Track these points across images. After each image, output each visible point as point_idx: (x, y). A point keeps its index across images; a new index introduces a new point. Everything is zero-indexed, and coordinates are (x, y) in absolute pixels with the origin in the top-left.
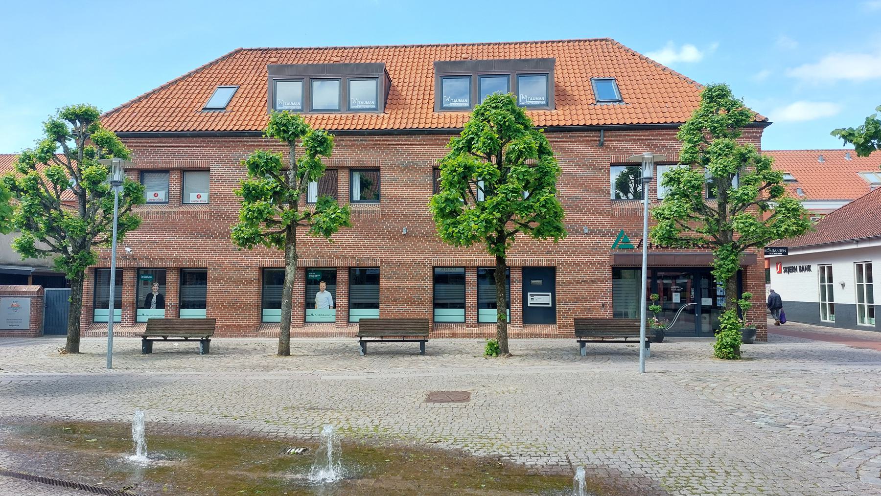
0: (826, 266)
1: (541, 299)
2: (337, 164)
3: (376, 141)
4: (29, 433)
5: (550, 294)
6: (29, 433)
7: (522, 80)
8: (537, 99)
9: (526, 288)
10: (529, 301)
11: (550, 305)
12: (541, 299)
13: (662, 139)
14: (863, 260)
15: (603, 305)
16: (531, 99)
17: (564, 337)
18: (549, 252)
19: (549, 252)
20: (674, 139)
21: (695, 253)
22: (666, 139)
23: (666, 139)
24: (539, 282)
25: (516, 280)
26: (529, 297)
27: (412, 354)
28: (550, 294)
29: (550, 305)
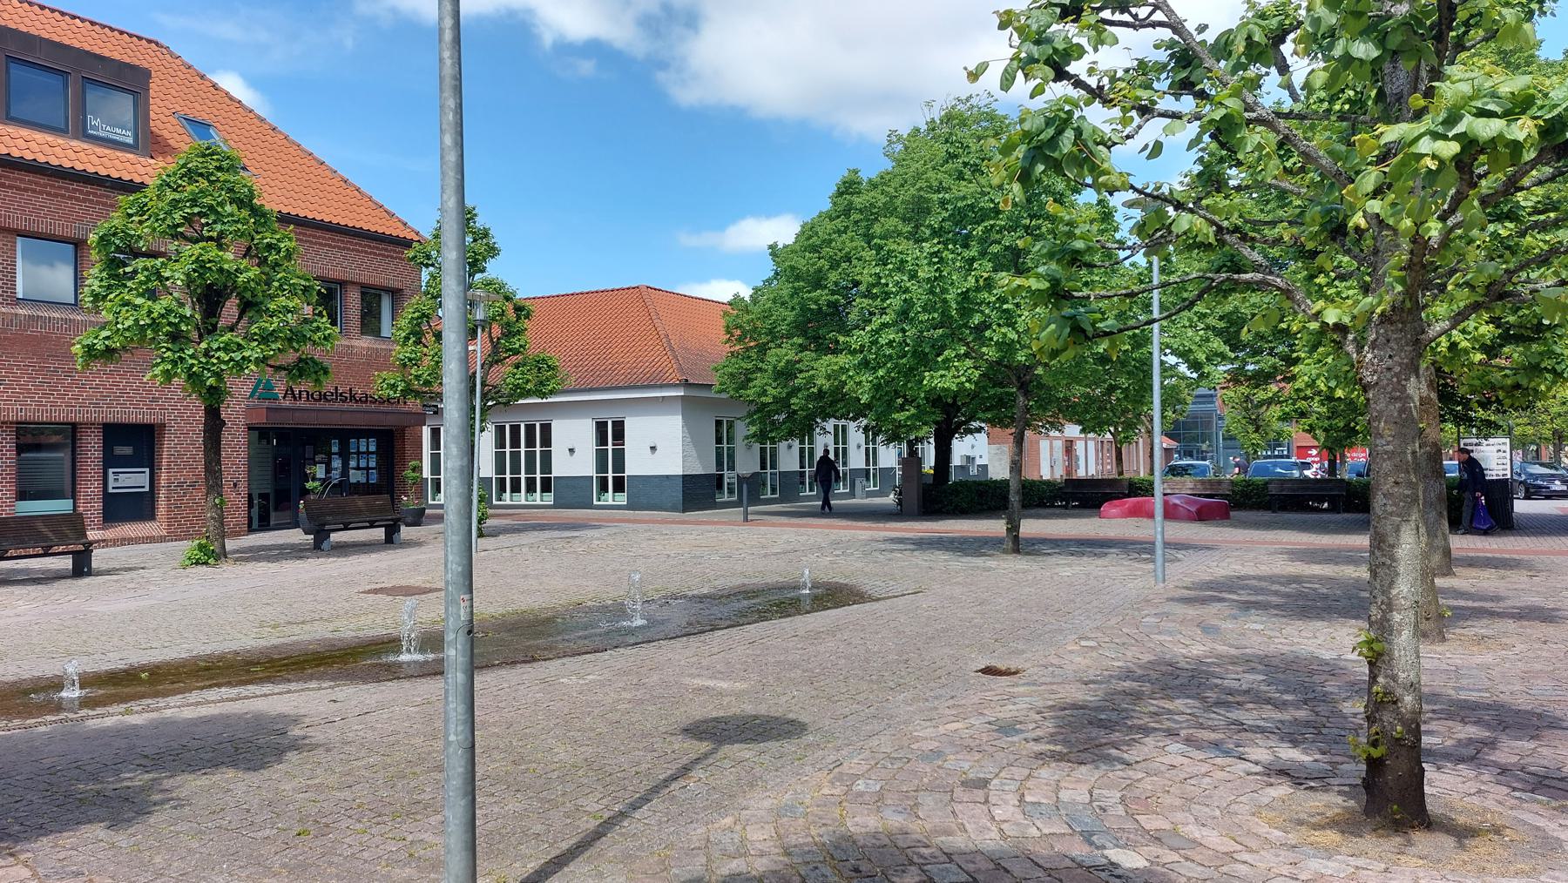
0: (725, 420)
1: (131, 480)
2: (348, 277)
3: (60, 187)
4: (1439, 370)
5: (147, 470)
6: (1439, 370)
7: (93, 96)
8: (119, 131)
9: (110, 461)
10: (111, 484)
11: (147, 489)
12: (131, 480)
13: (316, 243)
14: (609, 417)
15: (235, 485)
16: (108, 128)
17: (176, 540)
18: (155, 400)
19: (155, 400)
20: (401, 259)
21: (351, 409)
22: (321, 244)
23: (321, 244)
24: (127, 451)
25: (92, 447)
26: (111, 477)
27: (58, 576)
28: (147, 470)
29: (147, 489)
